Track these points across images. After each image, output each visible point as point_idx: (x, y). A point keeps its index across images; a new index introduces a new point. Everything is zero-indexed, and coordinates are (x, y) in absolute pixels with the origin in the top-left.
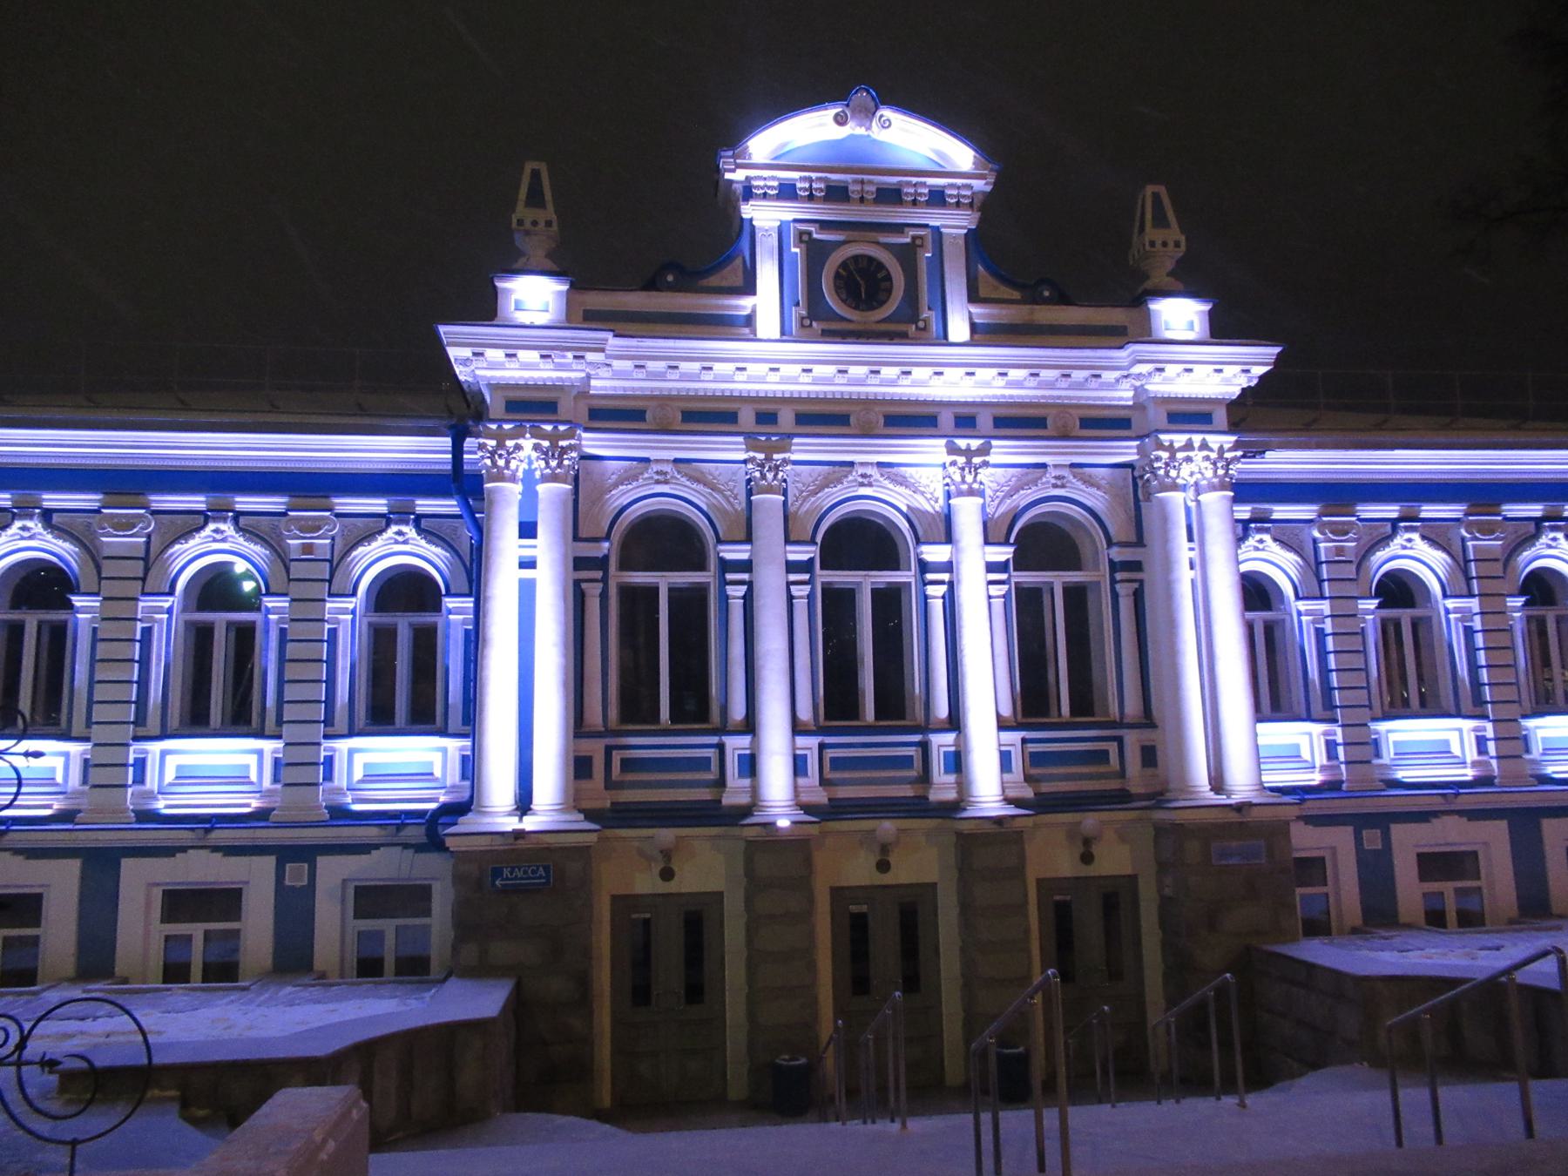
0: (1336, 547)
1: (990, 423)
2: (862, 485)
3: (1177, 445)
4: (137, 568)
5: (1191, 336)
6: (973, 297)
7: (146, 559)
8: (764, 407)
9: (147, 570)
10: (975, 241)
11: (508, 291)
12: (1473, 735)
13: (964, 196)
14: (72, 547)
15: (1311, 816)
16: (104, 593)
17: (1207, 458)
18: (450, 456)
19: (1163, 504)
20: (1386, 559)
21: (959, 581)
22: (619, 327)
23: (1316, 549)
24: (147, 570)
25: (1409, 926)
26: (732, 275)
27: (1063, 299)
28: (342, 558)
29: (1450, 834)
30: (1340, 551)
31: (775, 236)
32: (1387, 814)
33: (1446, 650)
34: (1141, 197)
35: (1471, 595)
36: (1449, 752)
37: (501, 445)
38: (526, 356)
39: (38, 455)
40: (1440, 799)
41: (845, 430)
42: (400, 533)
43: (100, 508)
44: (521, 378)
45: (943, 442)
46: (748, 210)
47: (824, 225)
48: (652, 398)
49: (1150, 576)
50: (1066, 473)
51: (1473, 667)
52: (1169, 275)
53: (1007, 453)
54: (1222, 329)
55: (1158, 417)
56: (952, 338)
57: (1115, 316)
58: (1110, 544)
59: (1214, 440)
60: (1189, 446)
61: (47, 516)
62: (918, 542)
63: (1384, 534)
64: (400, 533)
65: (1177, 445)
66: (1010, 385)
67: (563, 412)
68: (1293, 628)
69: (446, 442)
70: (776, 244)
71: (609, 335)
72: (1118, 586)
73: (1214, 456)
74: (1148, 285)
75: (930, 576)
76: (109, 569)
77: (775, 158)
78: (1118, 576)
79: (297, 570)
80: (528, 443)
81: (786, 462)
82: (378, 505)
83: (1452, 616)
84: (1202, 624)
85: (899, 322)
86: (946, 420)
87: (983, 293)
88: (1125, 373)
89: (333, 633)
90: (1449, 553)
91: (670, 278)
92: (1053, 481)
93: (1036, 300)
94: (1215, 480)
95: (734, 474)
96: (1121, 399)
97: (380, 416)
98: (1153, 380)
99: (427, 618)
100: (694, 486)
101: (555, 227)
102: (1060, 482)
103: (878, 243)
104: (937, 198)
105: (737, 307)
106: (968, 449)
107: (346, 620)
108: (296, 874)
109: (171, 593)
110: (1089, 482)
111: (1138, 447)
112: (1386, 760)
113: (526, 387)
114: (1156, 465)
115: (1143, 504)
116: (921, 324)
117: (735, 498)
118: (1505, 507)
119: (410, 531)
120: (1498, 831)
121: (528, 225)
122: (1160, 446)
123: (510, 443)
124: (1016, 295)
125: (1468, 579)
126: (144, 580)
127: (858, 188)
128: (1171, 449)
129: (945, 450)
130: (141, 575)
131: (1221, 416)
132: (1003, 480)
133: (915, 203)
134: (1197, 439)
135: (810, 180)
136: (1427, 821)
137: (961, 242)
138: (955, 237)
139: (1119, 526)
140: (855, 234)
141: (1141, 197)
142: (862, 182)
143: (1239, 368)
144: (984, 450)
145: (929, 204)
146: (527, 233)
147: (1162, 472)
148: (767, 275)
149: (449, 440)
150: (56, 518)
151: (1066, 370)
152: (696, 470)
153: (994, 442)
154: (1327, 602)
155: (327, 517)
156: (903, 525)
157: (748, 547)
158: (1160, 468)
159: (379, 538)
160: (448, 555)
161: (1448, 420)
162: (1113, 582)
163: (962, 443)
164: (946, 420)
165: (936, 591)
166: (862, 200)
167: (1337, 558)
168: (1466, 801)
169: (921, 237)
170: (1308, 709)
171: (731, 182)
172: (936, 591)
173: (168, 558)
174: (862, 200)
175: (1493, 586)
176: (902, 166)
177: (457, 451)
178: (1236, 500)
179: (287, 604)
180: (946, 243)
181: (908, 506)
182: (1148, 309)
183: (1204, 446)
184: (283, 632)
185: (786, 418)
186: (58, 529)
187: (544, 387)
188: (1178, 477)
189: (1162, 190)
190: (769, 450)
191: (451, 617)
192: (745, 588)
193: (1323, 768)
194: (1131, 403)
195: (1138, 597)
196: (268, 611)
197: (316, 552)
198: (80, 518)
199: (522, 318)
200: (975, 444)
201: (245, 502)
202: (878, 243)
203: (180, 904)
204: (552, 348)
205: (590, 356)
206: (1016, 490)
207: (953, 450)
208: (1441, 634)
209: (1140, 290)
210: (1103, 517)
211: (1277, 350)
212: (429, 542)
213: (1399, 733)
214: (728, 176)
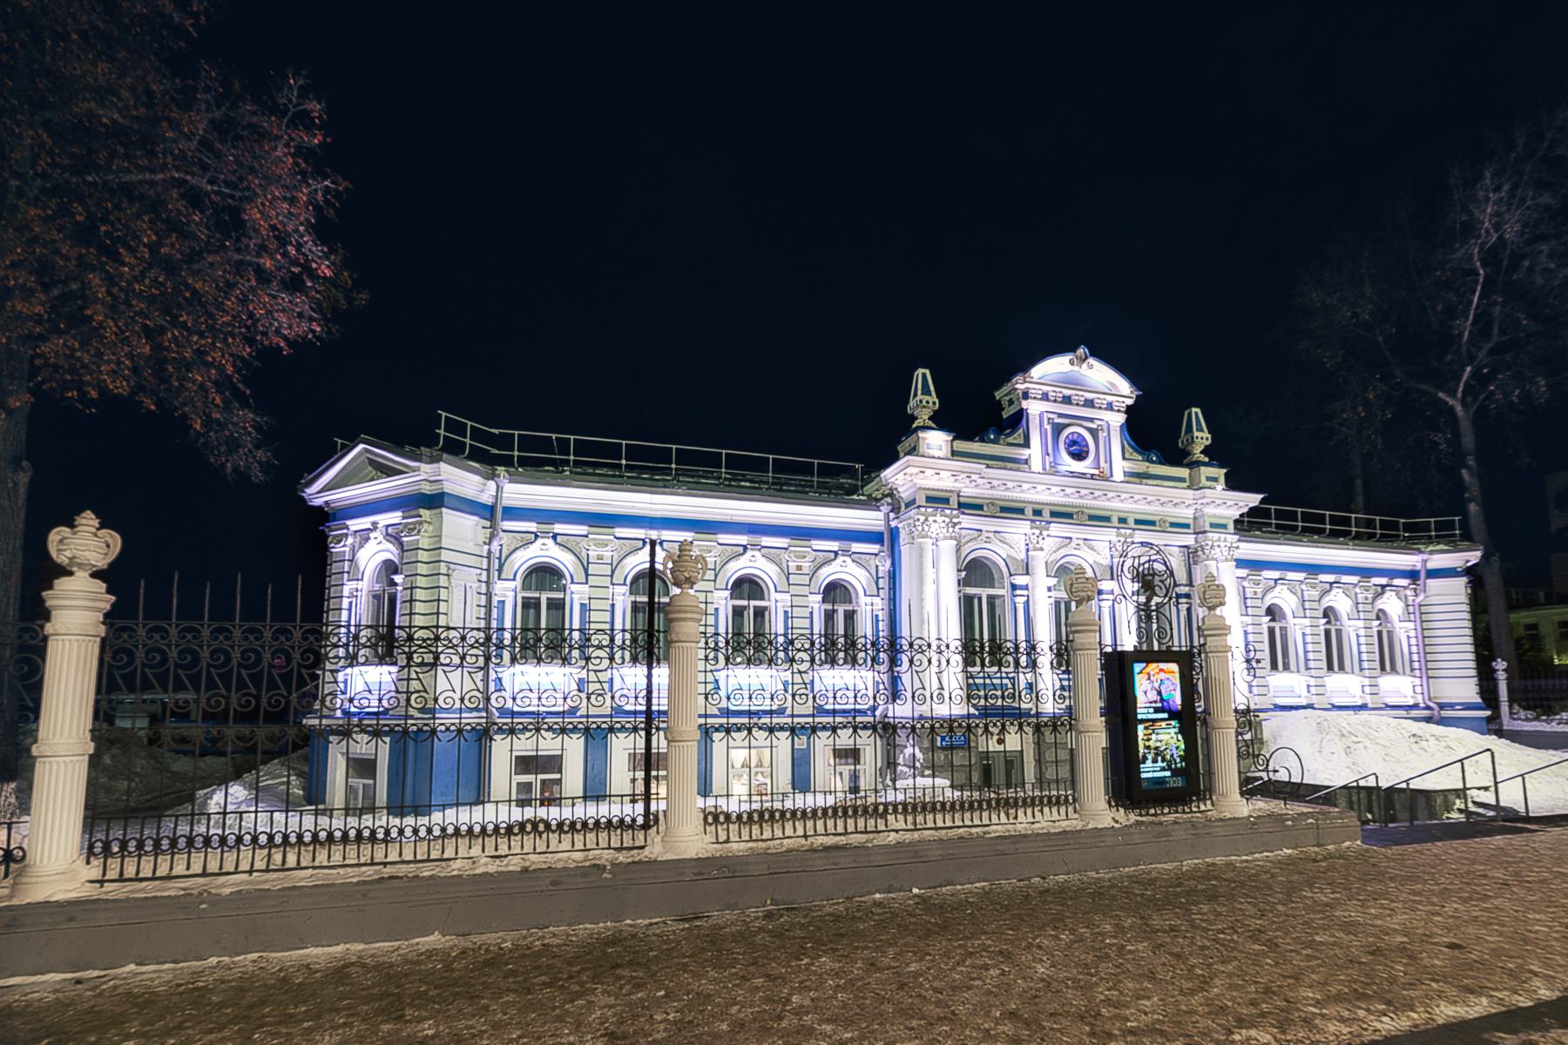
1: (1048, 514)
7: (611, 564)
8: (1036, 507)
16: (590, 583)
20: (1328, 601)
23: (1356, 598)
26: (1017, 437)
37: (926, 520)
38: (944, 474)
46: (1025, 404)
50: (1081, 542)
52: (1201, 452)
59: (1230, 537)
60: (1219, 540)
62: (1011, 575)
64: (544, 544)
66: (1051, 494)
75: (1018, 592)
80: (939, 519)
82: (834, 545)
87: (1127, 456)
101: (937, 405)
102: (1078, 547)
108: (801, 743)
121: (924, 403)
123: (931, 519)
134: (1223, 536)
145: (1106, 409)
146: (924, 407)
154: (1308, 620)
156: (1002, 564)
164: (1115, 520)
165: (1020, 601)
172: (1020, 601)
175: (1315, 613)
178: (1237, 567)
180: (1111, 428)
181: (1008, 556)
183: (1225, 540)
185: (1046, 513)
186: (560, 545)
189: (927, 372)
190: (1041, 529)
192: (1026, 598)
201: (767, 541)
203: (525, 764)
205: (974, 477)
214: (1018, 386)
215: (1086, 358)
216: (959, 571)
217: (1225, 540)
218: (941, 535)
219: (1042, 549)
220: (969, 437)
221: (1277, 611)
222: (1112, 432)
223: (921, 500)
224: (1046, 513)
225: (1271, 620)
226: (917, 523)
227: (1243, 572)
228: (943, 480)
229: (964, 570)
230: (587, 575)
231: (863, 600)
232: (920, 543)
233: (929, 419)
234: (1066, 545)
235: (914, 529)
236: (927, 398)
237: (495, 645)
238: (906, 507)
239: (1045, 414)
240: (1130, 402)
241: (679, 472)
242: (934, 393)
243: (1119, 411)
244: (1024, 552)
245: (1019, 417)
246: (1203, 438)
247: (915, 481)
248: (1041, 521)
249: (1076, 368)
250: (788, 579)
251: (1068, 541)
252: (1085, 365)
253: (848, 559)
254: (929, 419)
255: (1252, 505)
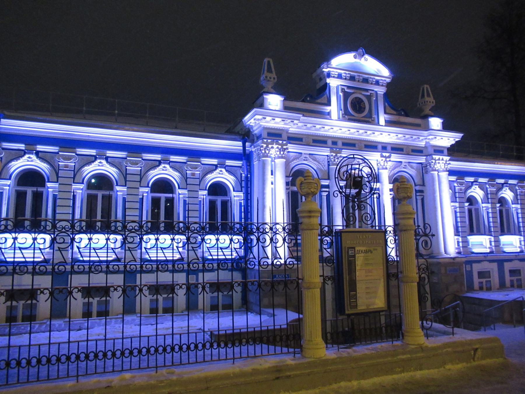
0: (65, 165)
1: (390, 149)
2: (304, 160)
3: (436, 159)
4: (138, 178)
5: (277, 109)
6: (385, 113)
7: (140, 175)
8: (334, 140)
9: (141, 179)
10: (386, 95)
11: (267, 99)
12: (489, 240)
13: (384, 83)
14: (47, 165)
15: (490, 260)
17: (278, 148)
18: (242, 148)
19: (432, 175)
20: (213, 177)
21: (382, 194)
22: (305, 114)
23: (241, 176)
24: (141, 179)
25: (477, 290)
26: (323, 100)
27: (407, 115)
28: (145, 174)
29: (485, 266)
30: (522, 192)
31: (335, 89)
32: (471, 261)
33: (482, 217)
34: (421, 89)
35: (489, 203)
36: (482, 245)
37: (267, 146)
38: (278, 120)
39: (102, 138)
40: (482, 257)
41: (301, 143)
42: (100, 163)
43: (58, 152)
44: (273, 126)
45: (380, 153)
46: (328, 81)
47: (349, 87)
48: (305, 135)
49: (427, 194)
51: (489, 222)
52: (430, 110)
53: (395, 157)
54: (446, 127)
55: (431, 151)
56: (381, 124)
57: (418, 121)
58: (415, 185)
60: (439, 159)
61: (37, 153)
63: (470, 186)
64: (29, 158)
65: (436, 159)
67: (263, 136)
68: (481, 211)
69: (240, 143)
70: (336, 92)
71: (301, 115)
72: (417, 197)
73: (444, 162)
74: (265, 90)
76: (129, 178)
77: (336, 66)
78: (418, 194)
79: (189, 181)
80: (275, 146)
81: (341, 156)
82: (214, 161)
83: (180, 196)
84: (274, 201)
85: (366, 118)
86: (380, 147)
87: (387, 111)
88: (425, 138)
89: (74, 196)
90: (182, 174)
91: (308, 99)
92: (304, 159)
93: (400, 114)
94: (445, 169)
95: (324, 159)
96: (422, 145)
97: (218, 133)
98: (262, 121)
99: (40, 189)
100: (314, 162)
101: (276, 80)
103: (361, 94)
104: (377, 83)
105: (326, 109)
106: (386, 156)
107: (6, 189)
109: (10, 179)
110: (412, 167)
111: (426, 158)
112: (470, 246)
113: (274, 129)
114: (262, 149)
115: (424, 175)
116: (373, 119)
117: (325, 166)
118: (497, 180)
119: (104, 162)
120: (495, 266)
122: (433, 159)
123: (270, 146)
124: (395, 113)
125: (518, 200)
126: (140, 182)
127: (358, 77)
128: (435, 160)
129: (380, 156)
130: (139, 180)
131: (446, 151)
132: (391, 165)
133: (372, 84)
134: (441, 157)
135: (346, 73)
136: (511, 261)
137: (382, 96)
138: (381, 94)
139: (418, 181)
140: (356, 91)
141: (421, 89)
142: (359, 76)
143: (453, 139)
144: (389, 157)
145: (375, 84)
146: (269, 81)
147: (432, 166)
148: (334, 100)
149: (241, 143)
150: (40, 154)
151: (305, 123)
152: (314, 157)
153: (392, 155)
155: (199, 165)
157: (329, 181)
158: (263, 150)
159: (21, 159)
160: (49, 166)
161: (466, 154)
162: (416, 196)
163: (384, 154)
164: (380, 147)
166: (359, 81)
167: (64, 169)
168: (489, 257)
169: (372, 93)
170: (485, 232)
171: (324, 71)
173: (9, 167)
174: (359, 81)
175: (494, 201)
176: (367, 72)
177: (244, 146)
178: (449, 175)
179: (126, 189)
182: (428, 121)
183: (443, 160)
184: (124, 199)
185: (340, 143)
187: (279, 130)
188: (269, 153)
190: (337, 153)
191: (118, 193)
192: (327, 193)
193: (489, 248)
194: (424, 146)
195: (423, 200)
196: (48, 188)
197: (195, 175)
198: (117, 160)
199: (270, 107)
200: (387, 155)
201: (173, 158)
202: (361, 94)
203: (156, 289)
204: (286, 118)
205: (296, 122)
206: (395, 168)
207: (382, 156)
208: (481, 212)
209: (262, 92)
210: (414, 177)
211: (462, 135)
212: (110, 166)
213: (505, 239)
214: (324, 70)
215: (364, 55)
216: (286, 177)
217: (443, 160)
218: (277, 156)
219: (386, 168)
220: (296, 99)
221: (474, 201)
222: (379, 98)
223: (265, 135)
224: (340, 143)
225: (469, 205)
226: (262, 149)
227: (453, 178)
228: (277, 124)
229: (291, 176)
230: (126, 181)
231: (234, 194)
232: (263, 160)
233: (272, 88)
234: (298, 158)
235: (260, 152)
236: (269, 75)
237: (145, 231)
238: (257, 140)
239: (340, 86)
240: (388, 80)
241: (119, 115)
242: (274, 73)
243: (382, 85)
244: (327, 166)
245: (326, 86)
246: (430, 101)
247: (261, 123)
248: (336, 148)
249: (357, 60)
250: (186, 181)
251: (300, 155)
252: (363, 59)
253: (223, 170)
254: (272, 88)
255: (457, 140)
